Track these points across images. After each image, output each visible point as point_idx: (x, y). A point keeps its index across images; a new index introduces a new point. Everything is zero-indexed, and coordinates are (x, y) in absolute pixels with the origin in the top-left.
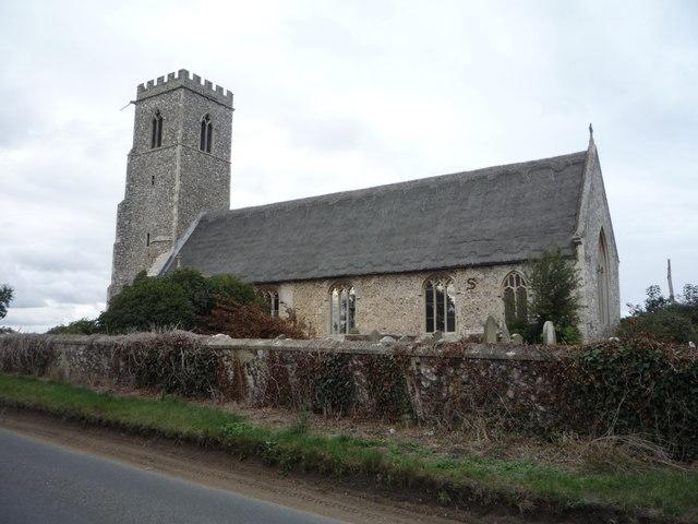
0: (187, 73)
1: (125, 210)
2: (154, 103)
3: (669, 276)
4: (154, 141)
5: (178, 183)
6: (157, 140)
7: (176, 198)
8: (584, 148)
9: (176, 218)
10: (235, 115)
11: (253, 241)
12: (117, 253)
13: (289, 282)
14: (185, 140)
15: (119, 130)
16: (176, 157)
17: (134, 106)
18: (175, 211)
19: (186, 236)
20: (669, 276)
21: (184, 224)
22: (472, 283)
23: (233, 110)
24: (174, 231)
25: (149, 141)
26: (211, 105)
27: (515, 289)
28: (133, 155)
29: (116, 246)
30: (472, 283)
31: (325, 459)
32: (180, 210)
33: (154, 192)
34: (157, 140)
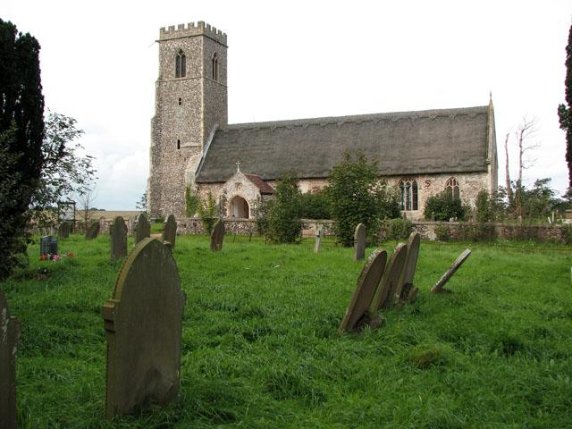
0: (204, 23)
1: (156, 122)
2: (177, 44)
3: (507, 167)
4: (177, 72)
5: (202, 105)
6: (181, 71)
7: (202, 116)
8: (487, 104)
9: (202, 131)
10: (229, 51)
11: (269, 149)
12: (154, 154)
13: (306, 179)
14: (205, 74)
15: (149, 66)
16: (196, 83)
17: (158, 44)
18: (202, 125)
19: (209, 143)
20: (507, 167)
21: (207, 135)
22: (428, 183)
23: (227, 47)
24: (201, 140)
25: (174, 72)
26: (216, 45)
27: (453, 187)
28: (160, 81)
29: (152, 149)
30: (428, 183)
31: (395, 311)
32: (205, 124)
33: (181, 110)
34: (181, 71)
